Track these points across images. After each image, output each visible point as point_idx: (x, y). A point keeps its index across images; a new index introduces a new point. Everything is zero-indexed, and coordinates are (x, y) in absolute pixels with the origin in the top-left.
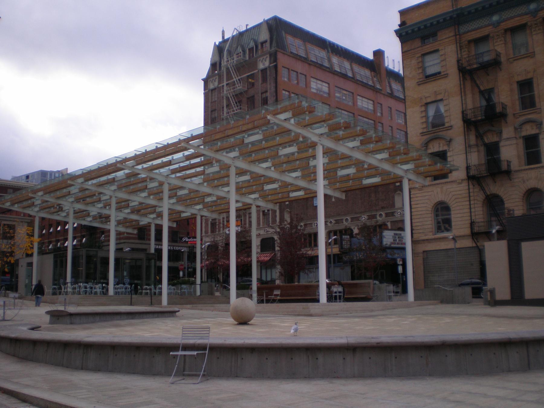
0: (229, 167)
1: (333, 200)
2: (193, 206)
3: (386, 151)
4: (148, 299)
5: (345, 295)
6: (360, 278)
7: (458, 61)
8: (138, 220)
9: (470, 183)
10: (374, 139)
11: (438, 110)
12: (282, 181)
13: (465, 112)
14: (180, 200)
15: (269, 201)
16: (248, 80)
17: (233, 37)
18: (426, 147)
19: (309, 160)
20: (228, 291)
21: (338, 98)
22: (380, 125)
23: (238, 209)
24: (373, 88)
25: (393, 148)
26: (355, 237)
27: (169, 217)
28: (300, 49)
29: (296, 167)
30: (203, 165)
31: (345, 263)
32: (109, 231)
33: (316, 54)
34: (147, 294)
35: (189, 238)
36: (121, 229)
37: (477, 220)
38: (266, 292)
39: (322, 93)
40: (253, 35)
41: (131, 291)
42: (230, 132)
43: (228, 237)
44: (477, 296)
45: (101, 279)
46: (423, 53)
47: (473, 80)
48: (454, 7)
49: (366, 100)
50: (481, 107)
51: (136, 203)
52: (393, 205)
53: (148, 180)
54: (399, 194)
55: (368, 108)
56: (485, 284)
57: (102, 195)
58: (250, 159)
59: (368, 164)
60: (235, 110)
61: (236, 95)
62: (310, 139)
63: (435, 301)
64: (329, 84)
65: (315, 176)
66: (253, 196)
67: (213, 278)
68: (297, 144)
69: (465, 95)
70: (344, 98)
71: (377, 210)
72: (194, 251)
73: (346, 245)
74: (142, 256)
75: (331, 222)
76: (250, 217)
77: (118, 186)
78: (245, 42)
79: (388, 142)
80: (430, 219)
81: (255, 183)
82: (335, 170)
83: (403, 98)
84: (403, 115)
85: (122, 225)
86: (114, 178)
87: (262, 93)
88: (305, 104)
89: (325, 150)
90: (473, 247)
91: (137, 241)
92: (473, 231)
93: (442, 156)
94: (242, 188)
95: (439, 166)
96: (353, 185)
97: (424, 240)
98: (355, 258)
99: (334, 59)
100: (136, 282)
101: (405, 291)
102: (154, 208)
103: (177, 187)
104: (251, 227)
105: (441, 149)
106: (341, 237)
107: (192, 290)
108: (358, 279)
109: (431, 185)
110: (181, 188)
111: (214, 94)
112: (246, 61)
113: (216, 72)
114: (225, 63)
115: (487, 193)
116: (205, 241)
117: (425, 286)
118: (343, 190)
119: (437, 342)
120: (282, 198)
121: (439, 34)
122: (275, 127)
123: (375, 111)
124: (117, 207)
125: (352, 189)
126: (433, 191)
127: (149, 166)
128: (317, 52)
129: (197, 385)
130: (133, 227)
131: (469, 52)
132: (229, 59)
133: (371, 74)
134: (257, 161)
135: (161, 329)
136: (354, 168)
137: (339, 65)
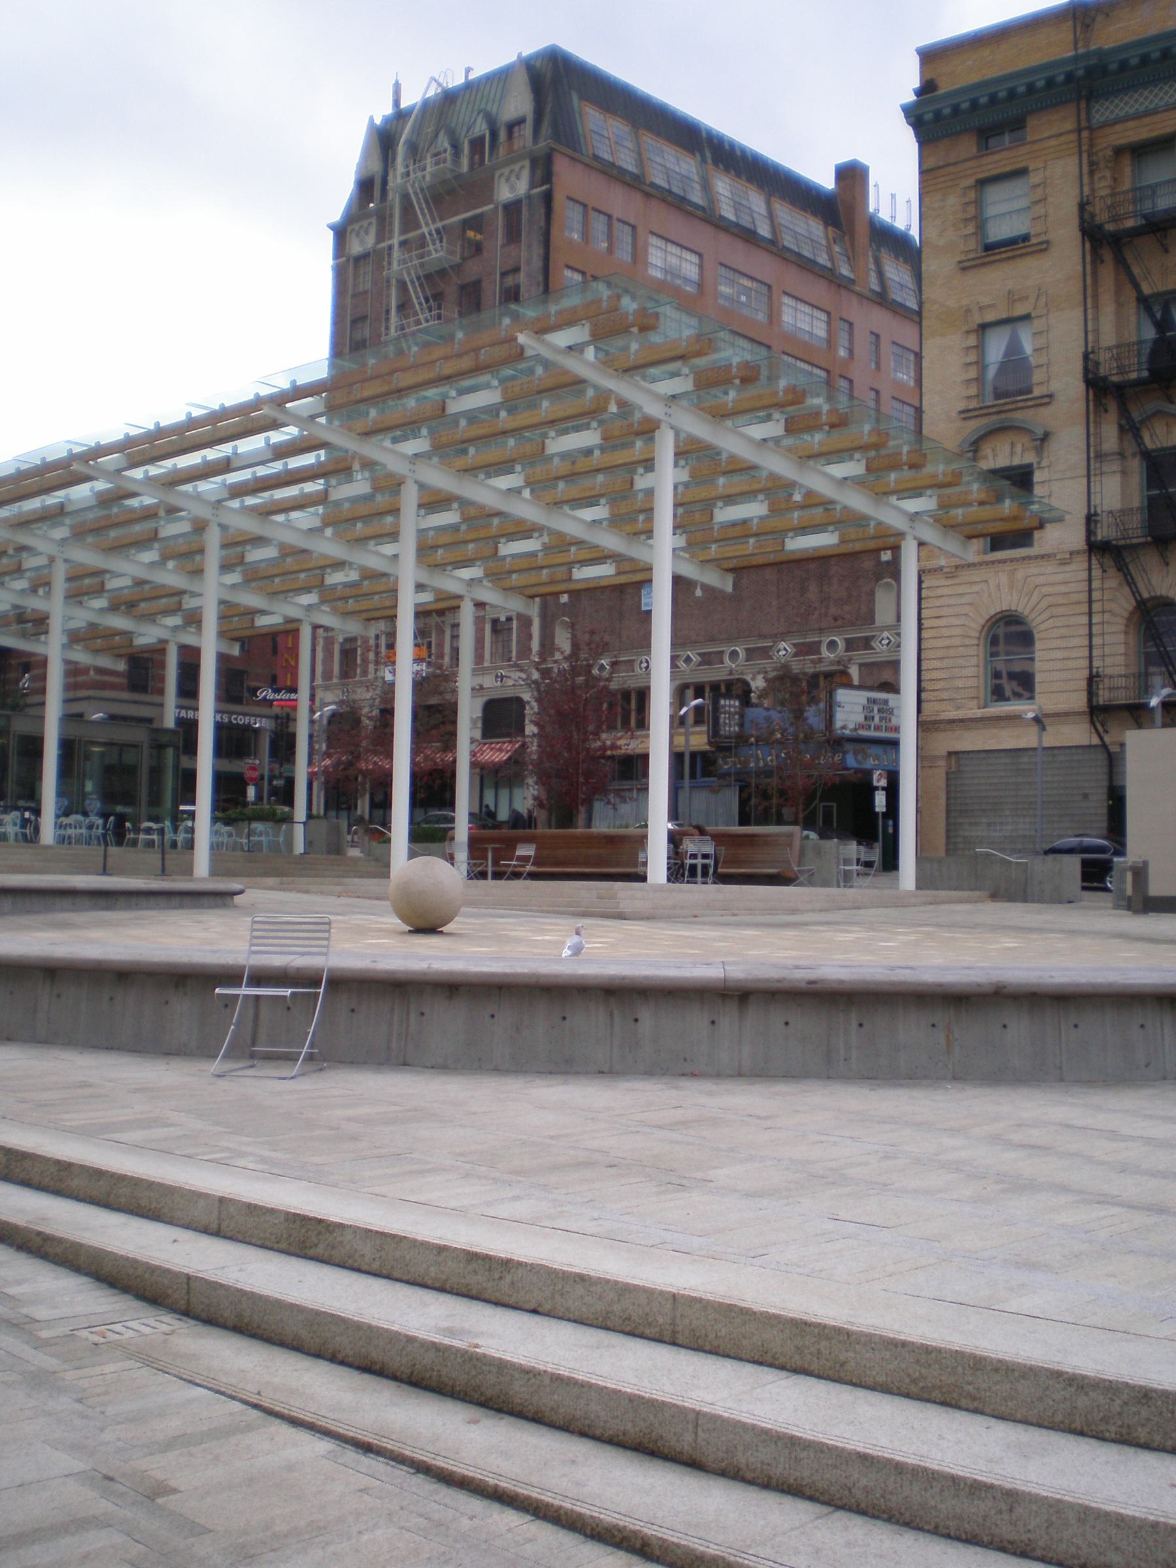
0: (399, 485)
1: (699, 593)
2: (291, 594)
3: (857, 456)
4: (154, 858)
5: (720, 865)
6: (764, 820)
7: (1082, 207)
8: (131, 633)
9: (1094, 561)
10: (824, 417)
11: (1014, 347)
12: (552, 533)
13: (1091, 356)
14: (255, 577)
15: (511, 589)
16: (464, 231)
17: (426, 104)
18: (975, 451)
19: (634, 471)
20: (385, 845)
21: (726, 298)
22: (843, 384)
23: (420, 609)
24: (829, 276)
25: (876, 446)
26: (757, 706)
27: (220, 625)
28: (621, 149)
29: (594, 493)
30: (324, 475)
31: (723, 776)
32: (44, 663)
33: (668, 165)
34: (150, 844)
35: (277, 691)
36: (81, 657)
37: (1108, 671)
38: (494, 850)
39: (678, 282)
40: (485, 100)
41: (104, 836)
42: (406, 380)
43: (389, 691)
44: (1095, 884)
45: (19, 797)
46: (981, 176)
47: (1121, 263)
48: (1080, 45)
49: (807, 309)
50: (1140, 342)
51: (125, 582)
52: (870, 618)
53: (162, 513)
54: (888, 585)
55: (811, 334)
56: (1121, 852)
57: (24, 555)
58: (460, 463)
59: (803, 491)
60: (423, 321)
61: (428, 277)
62: (641, 408)
63: (977, 893)
64: (700, 256)
65: (650, 520)
66: (466, 573)
67: (342, 809)
68: (601, 423)
69: (1096, 307)
70: (743, 298)
71: (821, 630)
72: (291, 729)
73: (730, 727)
74: (139, 735)
75: (688, 660)
76: (455, 637)
77: (72, 527)
78: (461, 119)
79: (867, 428)
80: (974, 661)
81: (473, 536)
82: (708, 506)
83: (915, 307)
84: (912, 357)
85: (82, 643)
86: (62, 506)
87: (503, 274)
88: (629, 305)
89: (682, 444)
90: (1090, 746)
91: (125, 695)
92: (1094, 700)
93: (1021, 478)
94: (435, 547)
95: (1008, 506)
96: (755, 551)
97: (952, 722)
98: (752, 765)
99: (719, 183)
100: (120, 809)
101: (891, 862)
102: (176, 598)
103: (247, 538)
104: (457, 665)
105: (1017, 461)
106: (716, 703)
107: (281, 839)
108: (758, 823)
109: (981, 564)
110: (259, 541)
111: (362, 272)
112: (458, 177)
113: (371, 205)
114: (399, 180)
115: (1140, 595)
116: (321, 700)
117: (947, 850)
118: (727, 565)
119: (979, 985)
120: (552, 582)
121: (1032, 122)
122: (539, 371)
123: (831, 342)
124: (67, 590)
125: (754, 563)
126: (986, 581)
127: (163, 470)
128: (671, 159)
129: (291, 1082)
130: (116, 652)
131: (1115, 180)
132: (411, 168)
133: (826, 233)
134: (481, 467)
135: (189, 938)
136: (762, 501)
137: (735, 202)
